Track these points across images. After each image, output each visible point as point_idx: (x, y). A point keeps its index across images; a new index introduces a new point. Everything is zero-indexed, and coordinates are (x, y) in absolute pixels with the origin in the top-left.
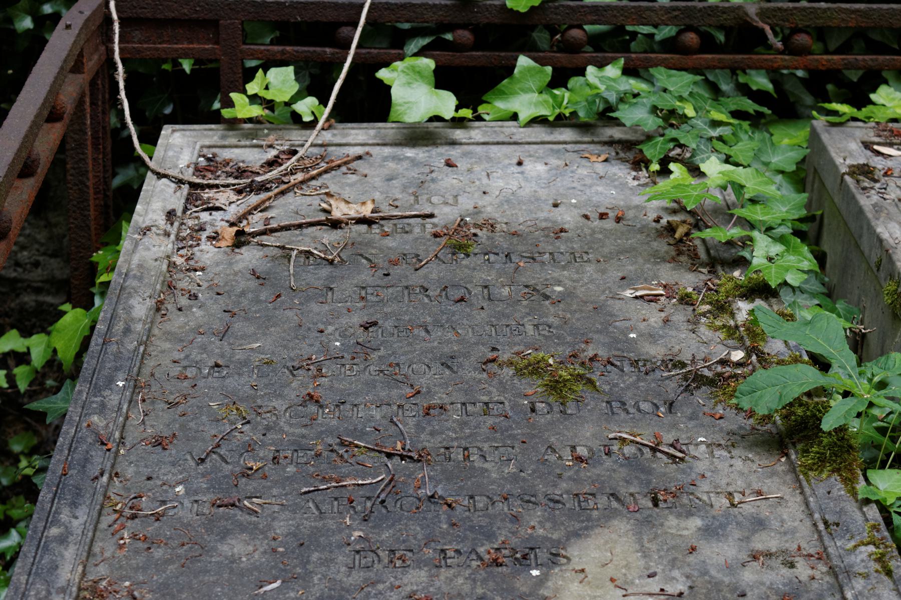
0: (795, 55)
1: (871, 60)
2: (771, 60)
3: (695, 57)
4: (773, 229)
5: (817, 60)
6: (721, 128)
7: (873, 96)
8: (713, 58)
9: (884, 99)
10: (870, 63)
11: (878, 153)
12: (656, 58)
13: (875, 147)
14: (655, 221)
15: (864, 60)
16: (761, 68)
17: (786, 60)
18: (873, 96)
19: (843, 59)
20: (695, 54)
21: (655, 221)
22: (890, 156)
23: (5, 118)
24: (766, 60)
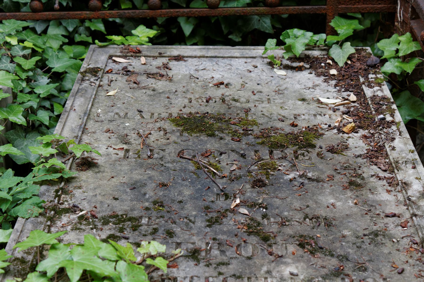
0: (93, 11)
1: (132, 12)
2: (80, 14)
3: (40, 13)
4: (25, 103)
5: (104, 14)
6: (26, 50)
7: (133, 32)
8: (49, 14)
9: (139, 32)
10: (132, 14)
11: (115, 61)
12: (19, 15)
13: (113, 58)
14: (258, 151)
15: (128, 13)
16: (75, 18)
17: (87, 14)
18: (133, 32)
19: (118, 13)
20: (40, 12)
21: (258, 151)
22: (120, 63)
23: (24, 164)
24: (77, 14)
